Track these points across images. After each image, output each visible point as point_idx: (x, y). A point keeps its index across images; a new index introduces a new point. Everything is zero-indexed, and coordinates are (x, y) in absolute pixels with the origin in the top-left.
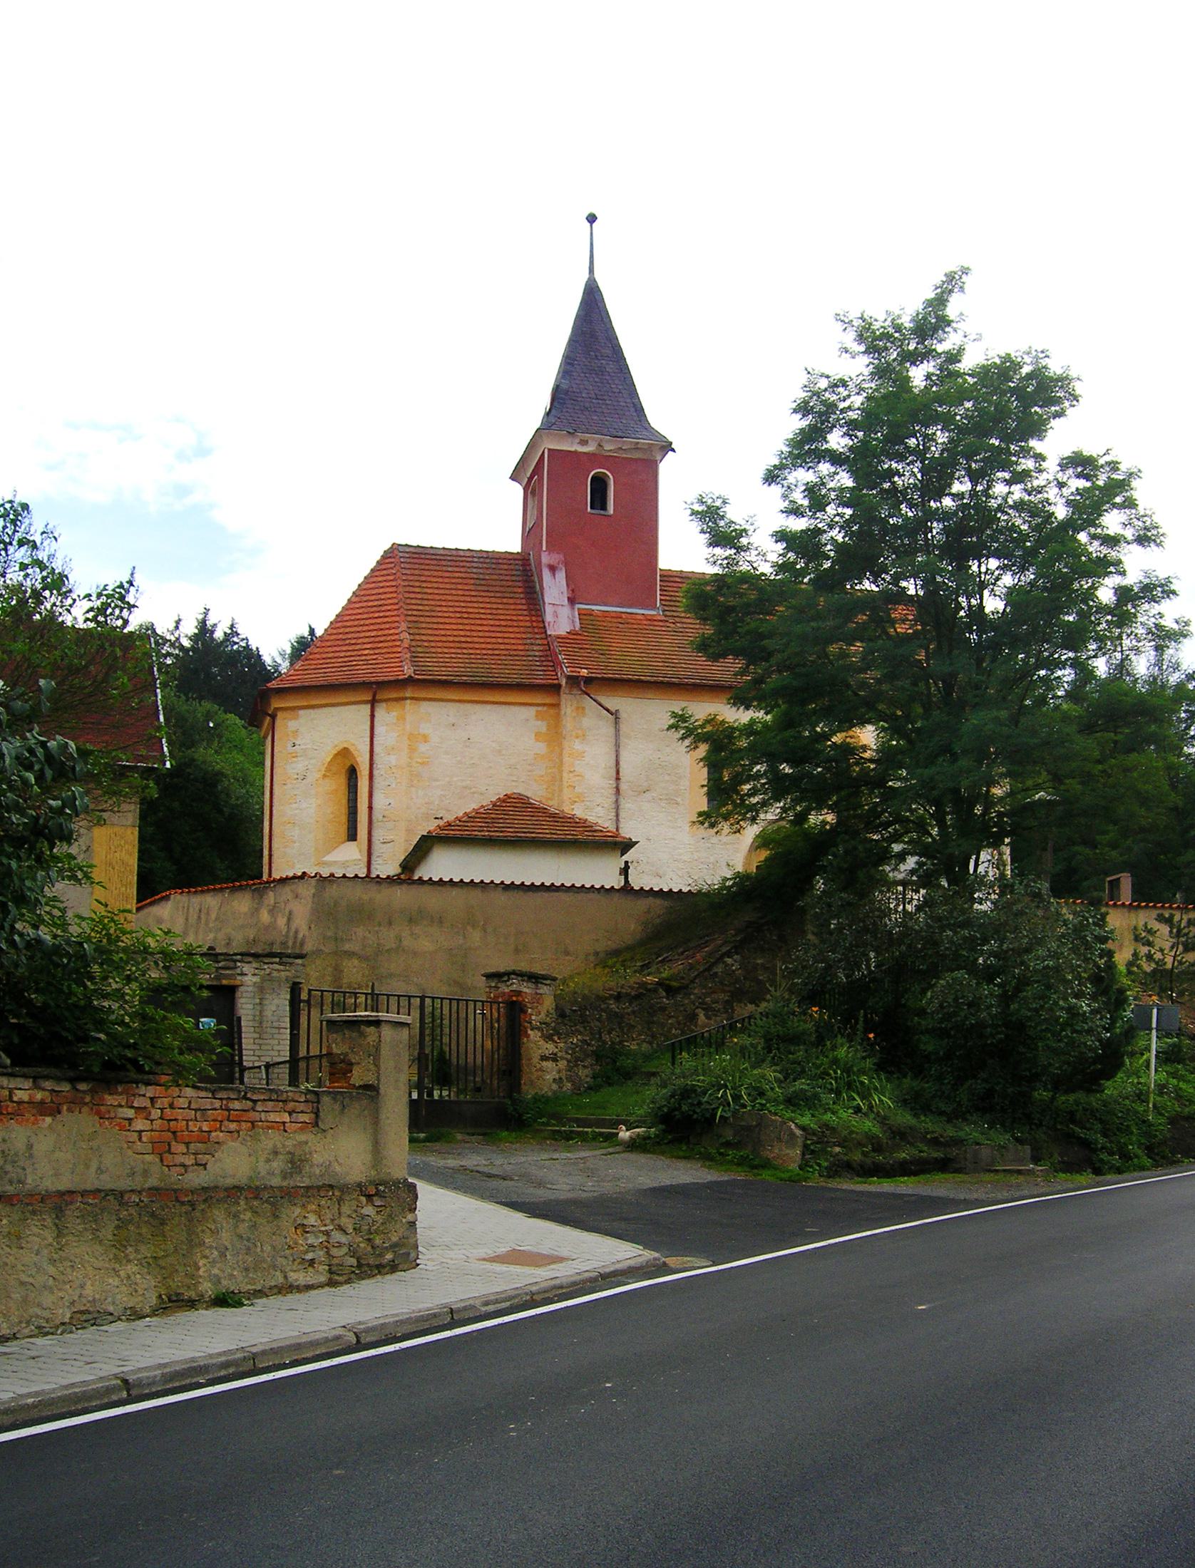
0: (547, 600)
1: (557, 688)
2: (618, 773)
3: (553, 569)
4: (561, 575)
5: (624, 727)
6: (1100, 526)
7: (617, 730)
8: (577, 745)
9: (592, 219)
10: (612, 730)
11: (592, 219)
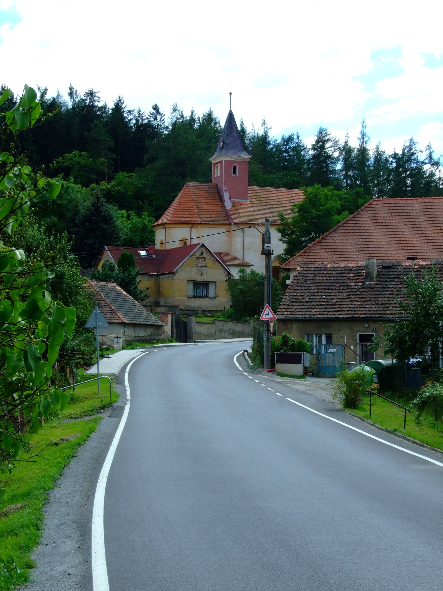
0: (225, 200)
1: (231, 224)
2: (244, 245)
3: (225, 191)
4: (227, 193)
5: (245, 234)
6: (286, 242)
7: (244, 234)
8: (235, 239)
9: (231, 94)
10: (242, 235)
11: (231, 94)
